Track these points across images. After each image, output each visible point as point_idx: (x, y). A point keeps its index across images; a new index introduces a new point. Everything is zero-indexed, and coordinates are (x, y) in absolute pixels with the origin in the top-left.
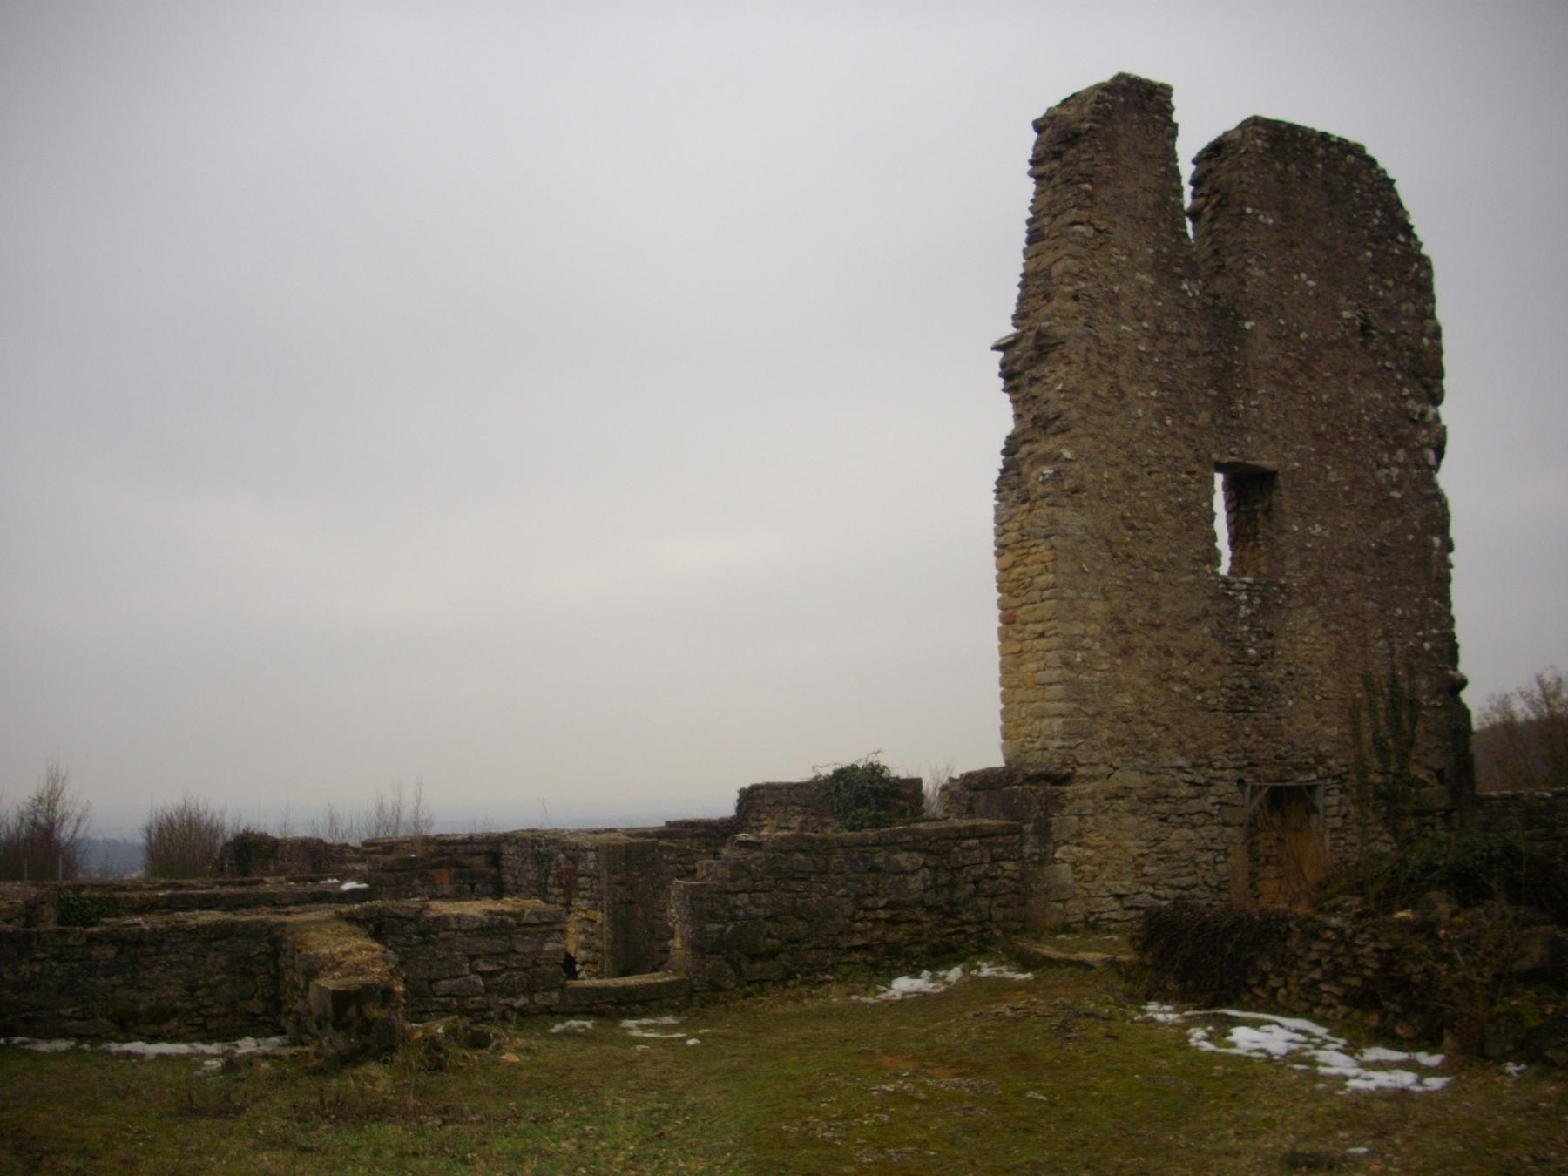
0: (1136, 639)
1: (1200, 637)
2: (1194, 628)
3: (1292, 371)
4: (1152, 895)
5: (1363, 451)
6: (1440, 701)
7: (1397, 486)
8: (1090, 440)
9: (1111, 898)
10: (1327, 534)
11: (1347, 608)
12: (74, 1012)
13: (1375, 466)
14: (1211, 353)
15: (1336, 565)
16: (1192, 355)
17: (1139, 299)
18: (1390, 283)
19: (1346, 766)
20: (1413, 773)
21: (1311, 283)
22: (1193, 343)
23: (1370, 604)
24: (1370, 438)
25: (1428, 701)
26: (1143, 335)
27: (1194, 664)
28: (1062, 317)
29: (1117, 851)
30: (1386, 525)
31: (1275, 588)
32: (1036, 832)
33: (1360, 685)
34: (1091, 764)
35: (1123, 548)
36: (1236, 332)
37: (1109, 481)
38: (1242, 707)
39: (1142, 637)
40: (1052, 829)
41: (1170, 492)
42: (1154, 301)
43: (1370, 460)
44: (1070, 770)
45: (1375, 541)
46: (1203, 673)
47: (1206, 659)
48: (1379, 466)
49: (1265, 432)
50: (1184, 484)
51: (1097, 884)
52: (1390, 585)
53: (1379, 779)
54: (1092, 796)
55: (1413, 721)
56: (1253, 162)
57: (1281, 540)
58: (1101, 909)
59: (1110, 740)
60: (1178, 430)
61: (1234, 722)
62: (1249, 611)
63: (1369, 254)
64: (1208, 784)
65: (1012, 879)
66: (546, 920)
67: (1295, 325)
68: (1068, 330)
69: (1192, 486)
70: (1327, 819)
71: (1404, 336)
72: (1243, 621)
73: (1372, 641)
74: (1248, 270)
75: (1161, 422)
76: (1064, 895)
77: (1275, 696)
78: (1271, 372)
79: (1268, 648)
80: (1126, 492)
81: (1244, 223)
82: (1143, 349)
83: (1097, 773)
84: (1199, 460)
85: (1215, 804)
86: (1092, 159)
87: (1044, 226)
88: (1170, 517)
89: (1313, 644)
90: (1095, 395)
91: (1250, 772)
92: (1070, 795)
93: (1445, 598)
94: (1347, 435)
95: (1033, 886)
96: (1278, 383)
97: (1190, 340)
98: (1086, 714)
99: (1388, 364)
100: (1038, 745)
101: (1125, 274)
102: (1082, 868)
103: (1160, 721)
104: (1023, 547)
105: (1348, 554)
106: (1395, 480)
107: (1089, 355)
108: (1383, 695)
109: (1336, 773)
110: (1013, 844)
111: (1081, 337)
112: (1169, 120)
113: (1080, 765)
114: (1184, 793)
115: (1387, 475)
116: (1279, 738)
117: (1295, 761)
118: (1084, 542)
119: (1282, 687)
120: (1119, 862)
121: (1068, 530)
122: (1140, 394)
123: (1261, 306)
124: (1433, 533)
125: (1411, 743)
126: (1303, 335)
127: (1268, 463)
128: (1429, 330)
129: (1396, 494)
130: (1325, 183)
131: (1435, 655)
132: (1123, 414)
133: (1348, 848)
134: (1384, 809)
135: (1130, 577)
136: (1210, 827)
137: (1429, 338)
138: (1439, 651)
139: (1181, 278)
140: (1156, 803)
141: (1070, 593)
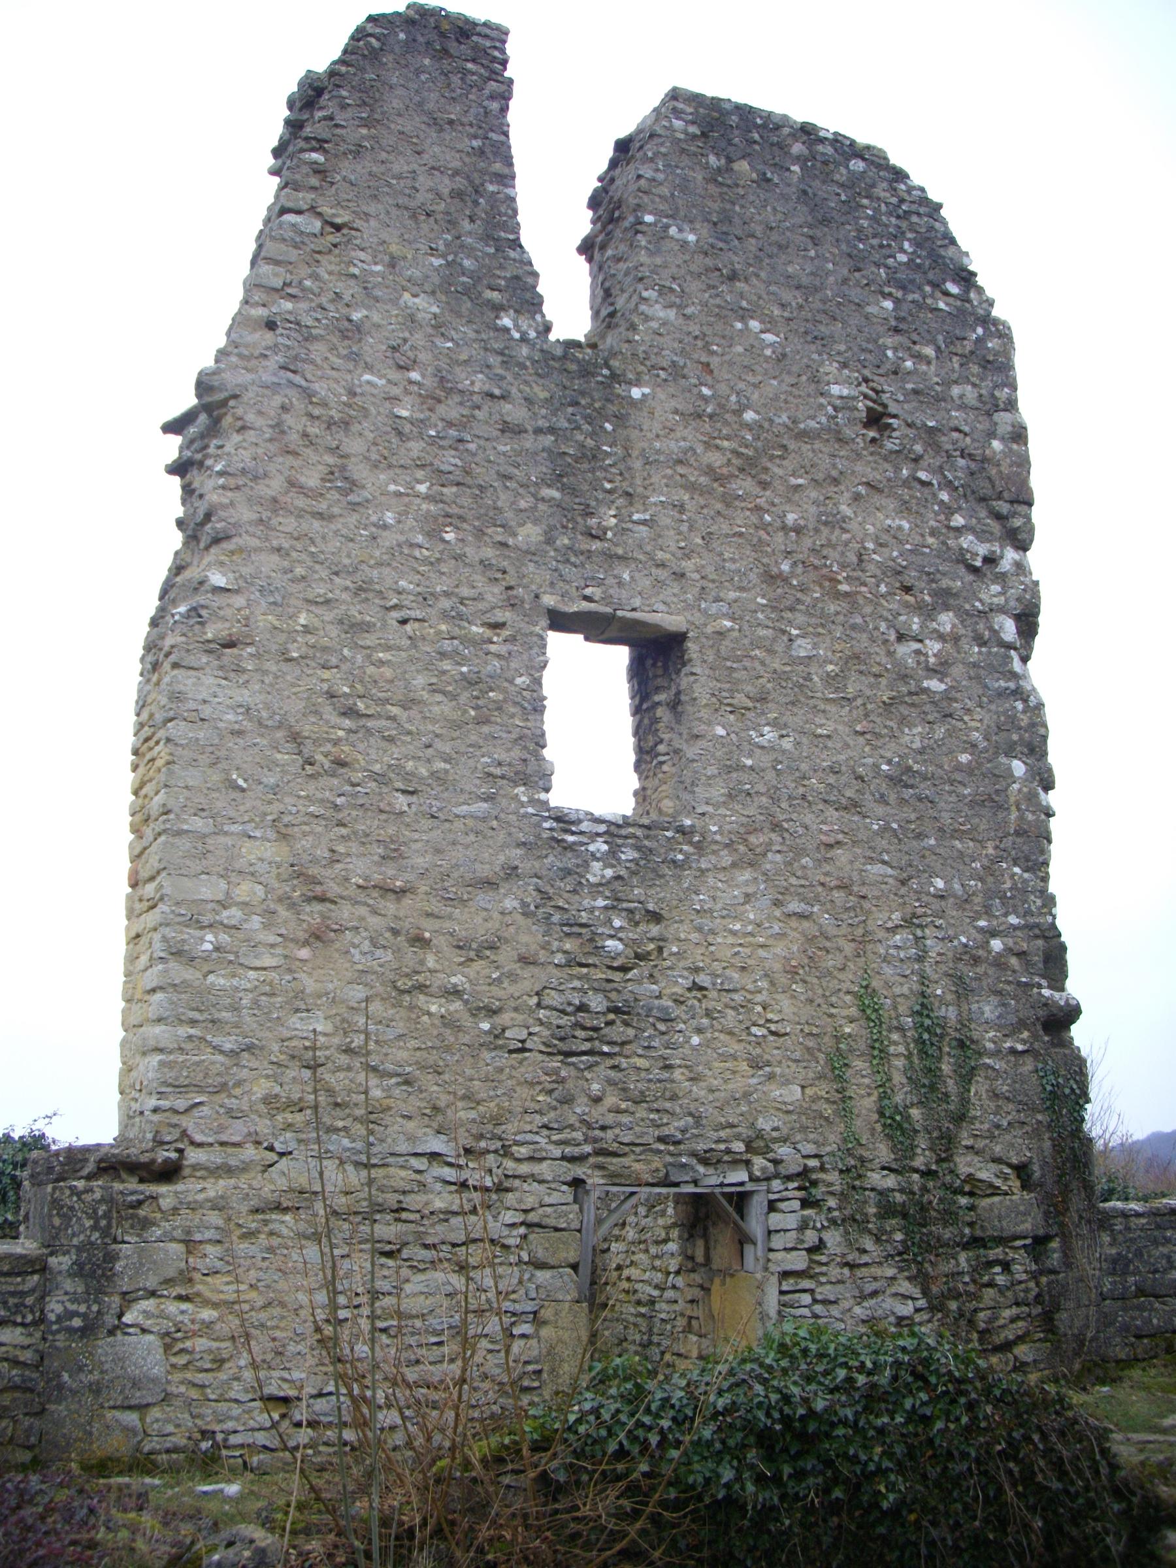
0: (345, 913)
1: (496, 915)
2: (482, 898)
5: (868, 610)
6: (1024, 1042)
7: (938, 671)
8: (275, 558)
9: (258, 1404)
10: (787, 744)
11: (827, 874)
13: (893, 637)
14: (552, 430)
15: (804, 797)
16: (509, 429)
17: (407, 335)
18: (929, 351)
19: (816, 1156)
20: (963, 1170)
21: (769, 337)
22: (514, 412)
23: (876, 869)
24: (883, 588)
26: (407, 392)
27: (478, 965)
28: (240, 356)
29: (276, 1311)
30: (914, 736)
31: (669, 834)
32: (78, 1270)
33: (853, 1011)
34: (222, 1144)
35: (329, 747)
36: (608, 400)
37: (307, 630)
38: (586, 1046)
39: (363, 911)
40: (118, 1267)
41: (443, 655)
42: (439, 342)
43: (883, 626)
44: (174, 1155)
45: (889, 762)
46: (499, 981)
47: (506, 956)
48: (901, 638)
49: (662, 565)
51: (223, 1376)
52: (920, 836)
53: (891, 1181)
54: (218, 1205)
55: (966, 1077)
56: (663, 150)
57: (691, 752)
58: (230, 1425)
59: (267, 1100)
60: (469, 551)
61: (563, 1073)
62: (609, 873)
63: (888, 304)
64: (500, 1189)
67: (733, 398)
68: (249, 377)
69: (493, 648)
70: (771, 1255)
71: (955, 435)
72: (597, 889)
73: (881, 934)
74: (643, 307)
75: (434, 534)
76: (137, 1397)
77: (662, 1027)
78: (681, 470)
79: (652, 940)
80: (346, 652)
81: (639, 237)
82: (405, 413)
83: (233, 1162)
85: (513, 1225)
86: (331, 118)
88: (439, 697)
89: (751, 934)
90: (292, 483)
91: (601, 1167)
92: (166, 1203)
93: (1038, 864)
94: (835, 581)
95: (66, 1376)
97: (508, 407)
98: (218, 1049)
99: (922, 475)
101: (378, 293)
102: (188, 1344)
103: (390, 1067)
105: (832, 779)
106: (932, 660)
107: (285, 416)
108: (901, 1029)
109: (795, 1169)
110: (22, 1294)
111: (274, 387)
114: (439, 1204)
115: (918, 652)
116: (668, 1105)
117: (701, 1146)
118: (239, 733)
119: (677, 1012)
120: (278, 1334)
121: (206, 711)
122: (392, 488)
123: (665, 365)
125: (960, 1118)
126: (749, 416)
127: (672, 621)
128: (1004, 429)
129: (935, 685)
130: (805, 192)
131: (1014, 961)
132: (353, 519)
133: (818, 1309)
134: (899, 1236)
135: (339, 801)
137: (1002, 439)
138: (1021, 954)
139: (498, 309)
141: (198, 824)
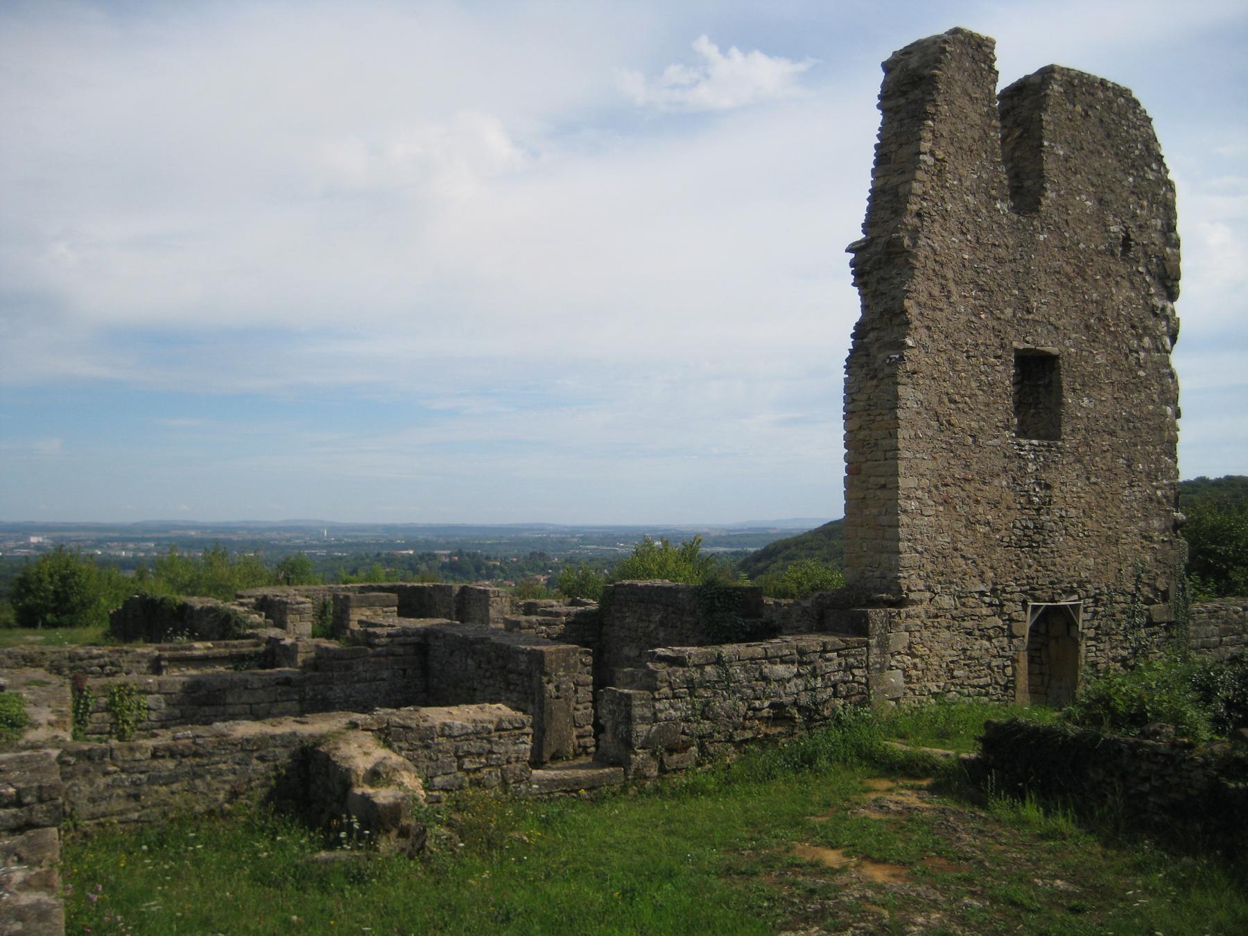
3: (1072, 275)
4: (959, 692)
12: (140, 817)
16: (1000, 261)
18: (1145, 203)
21: (1088, 203)
25: (1158, 537)
32: (879, 645)
50: (993, 366)
65: (860, 683)
66: (517, 725)
82: (966, 257)
84: (1002, 347)
87: (891, 152)
94: (1109, 326)
96: (1061, 284)
99: (1140, 269)
100: (877, 574)
104: (869, 415)
112: (991, 68)
113: (912, 591)
124: (1167, 404)
126: (1082, 246)
127: (1054, 350)
135: (952, 441)
136: (1001, 639)
139: (995, 199)
140: (964, 620)
